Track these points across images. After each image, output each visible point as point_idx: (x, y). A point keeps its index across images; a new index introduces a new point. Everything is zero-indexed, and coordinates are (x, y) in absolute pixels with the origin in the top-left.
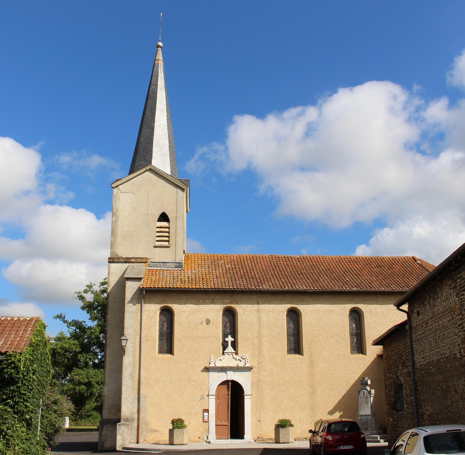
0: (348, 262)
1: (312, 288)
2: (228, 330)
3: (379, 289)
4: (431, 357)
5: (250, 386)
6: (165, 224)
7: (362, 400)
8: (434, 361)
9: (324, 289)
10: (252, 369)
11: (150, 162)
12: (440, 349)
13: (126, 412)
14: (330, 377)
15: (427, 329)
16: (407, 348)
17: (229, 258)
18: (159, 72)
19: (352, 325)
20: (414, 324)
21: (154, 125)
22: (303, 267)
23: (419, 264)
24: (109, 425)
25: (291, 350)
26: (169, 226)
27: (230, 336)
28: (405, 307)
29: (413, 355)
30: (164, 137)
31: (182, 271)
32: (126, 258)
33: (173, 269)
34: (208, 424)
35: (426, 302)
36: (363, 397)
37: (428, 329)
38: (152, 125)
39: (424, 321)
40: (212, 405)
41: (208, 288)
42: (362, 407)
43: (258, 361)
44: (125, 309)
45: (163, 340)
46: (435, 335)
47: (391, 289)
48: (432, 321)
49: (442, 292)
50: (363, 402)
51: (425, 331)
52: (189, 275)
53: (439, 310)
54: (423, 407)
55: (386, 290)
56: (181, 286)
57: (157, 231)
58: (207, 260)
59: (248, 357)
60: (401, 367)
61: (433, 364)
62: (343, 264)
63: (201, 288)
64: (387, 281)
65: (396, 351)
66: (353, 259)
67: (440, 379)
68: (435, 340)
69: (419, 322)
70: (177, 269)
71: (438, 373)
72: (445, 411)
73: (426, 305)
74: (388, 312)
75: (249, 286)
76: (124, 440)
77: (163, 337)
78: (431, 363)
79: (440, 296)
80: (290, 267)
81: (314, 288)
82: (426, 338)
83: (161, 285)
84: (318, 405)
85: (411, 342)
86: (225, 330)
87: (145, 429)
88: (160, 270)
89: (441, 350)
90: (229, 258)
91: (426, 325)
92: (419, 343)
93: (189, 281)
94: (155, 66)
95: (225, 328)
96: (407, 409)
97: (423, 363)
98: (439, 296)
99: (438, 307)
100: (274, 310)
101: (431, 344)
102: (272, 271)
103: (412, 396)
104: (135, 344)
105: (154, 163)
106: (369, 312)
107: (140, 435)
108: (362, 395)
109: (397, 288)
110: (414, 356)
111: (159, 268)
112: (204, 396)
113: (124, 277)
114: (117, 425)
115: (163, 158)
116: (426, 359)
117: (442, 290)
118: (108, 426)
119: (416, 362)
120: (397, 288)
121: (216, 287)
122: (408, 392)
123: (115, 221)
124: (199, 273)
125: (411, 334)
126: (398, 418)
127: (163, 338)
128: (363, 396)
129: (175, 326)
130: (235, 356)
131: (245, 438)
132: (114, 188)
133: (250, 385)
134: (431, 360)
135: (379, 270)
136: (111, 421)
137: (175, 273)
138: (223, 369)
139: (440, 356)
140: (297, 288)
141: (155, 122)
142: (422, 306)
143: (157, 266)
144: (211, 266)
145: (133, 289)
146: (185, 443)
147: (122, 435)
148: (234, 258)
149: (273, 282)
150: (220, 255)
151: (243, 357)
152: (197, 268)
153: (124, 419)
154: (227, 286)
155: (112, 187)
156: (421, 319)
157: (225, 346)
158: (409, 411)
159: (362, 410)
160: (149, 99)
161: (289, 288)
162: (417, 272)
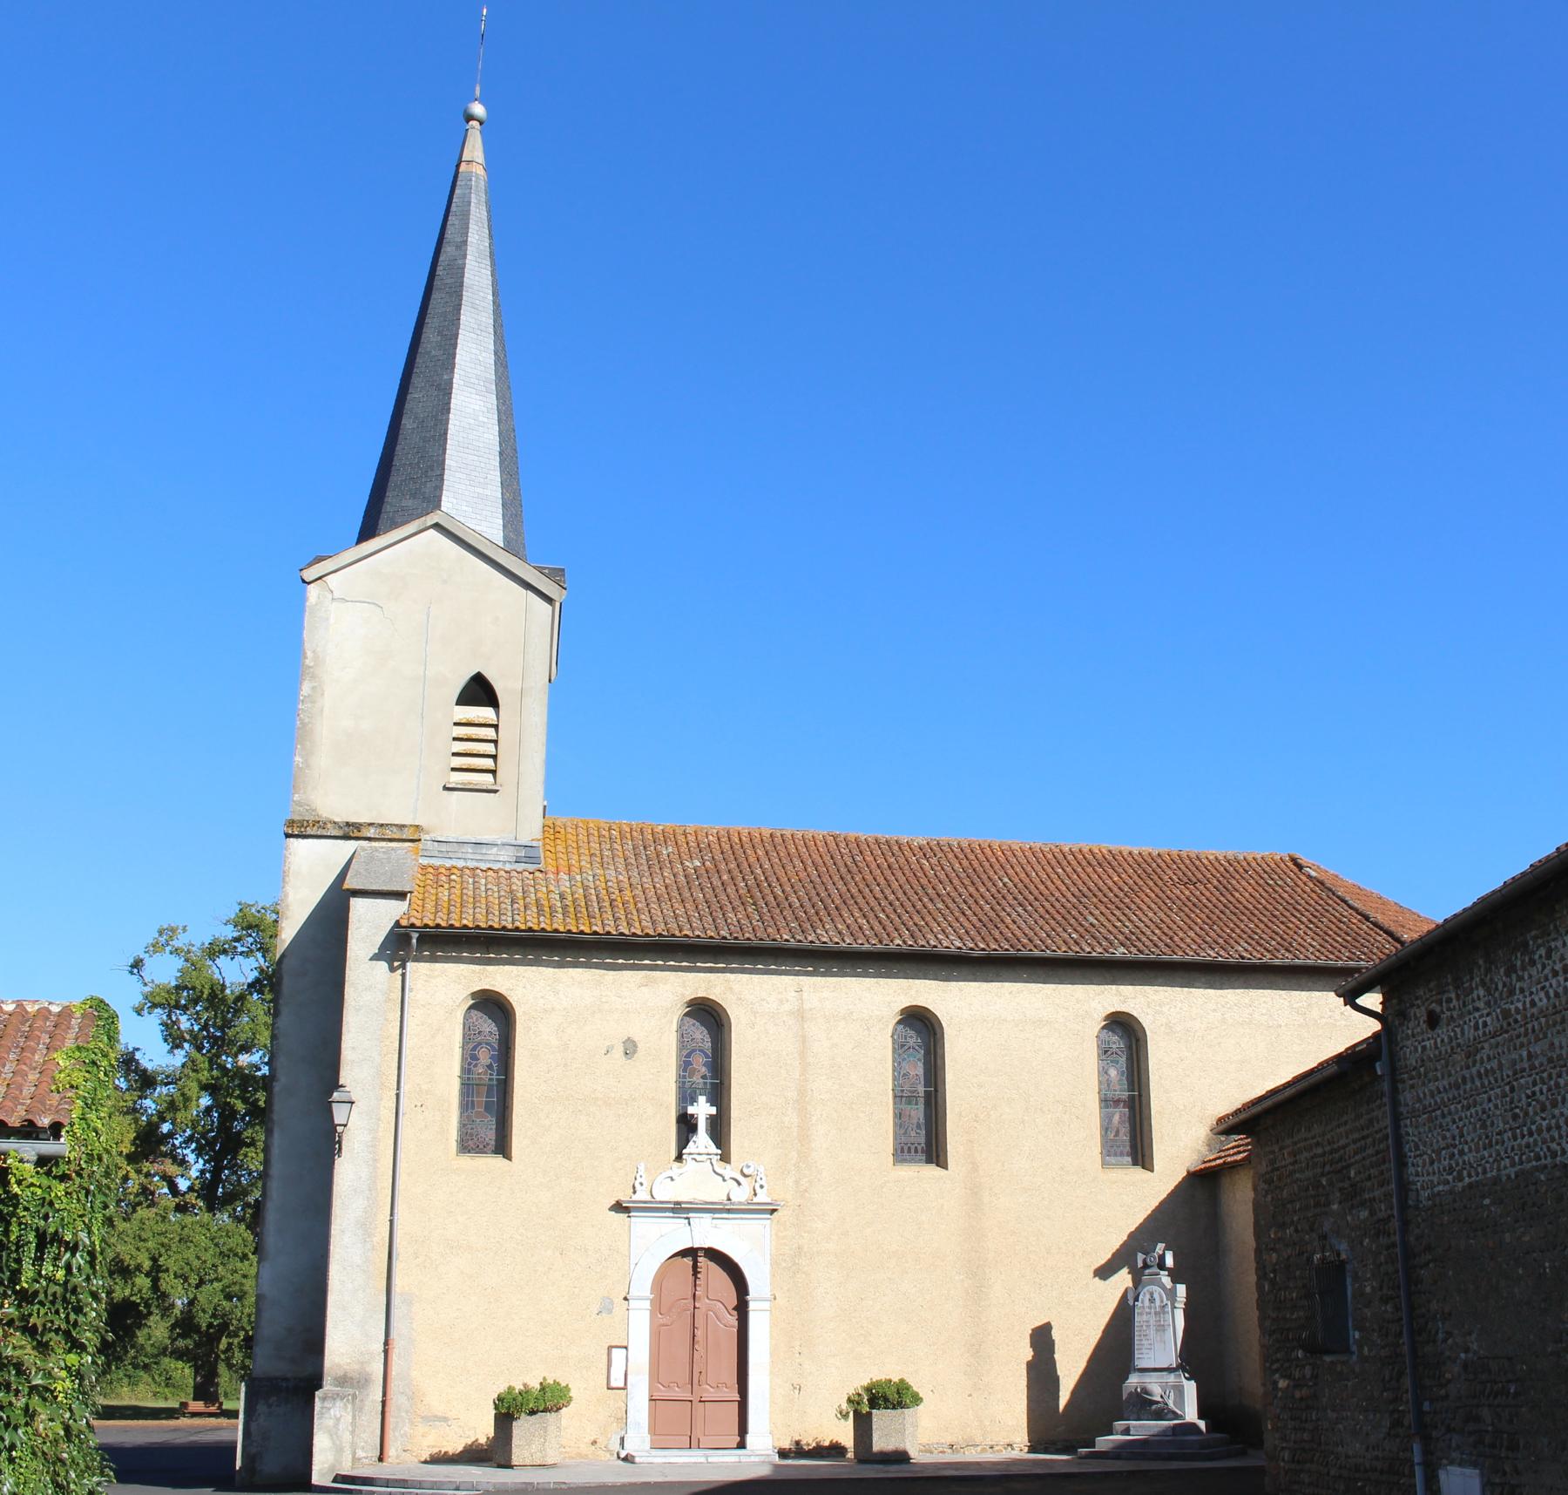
0: (1084, 863)
1: (982, 946)
2: (697, 1079)
3: (1198, 955)
4: (1488, 1166)
5: (767, 1268)
6: (486, 713)
7: (1145, 1318)
8: (1504, 1179)
9: (1008, 950)
10: (775, 1210)
11: (434, 502)
12: (1531, 1140)
13: (343, 1354)
14: (1034, 1243)
15: (1474, 1070)
16: (1370, 1139)
17: (693, 839)
18: (472, 204)
19: (1106, 1073)
20: (1410, 1055)
21: (452, 379)
22: (942, 876)
23: (1315, 878)
24: (275, 1398)
25: (913, 1151)
26: (498, 721)
27: (702, 1099)
28: (1373, 1000)
29: (1402, 1163)
30: (486, 420)
31: (537, 874)
32: (348, 824)
33: (508, 867)
34: (624, 1398)
35: (1472, 979)
36: (1148, 1310)
37: (1479, 1072)
38: (445, 377)
39: (1459, 1045)
40: (639, 1326)
41: (634, 935)
42: (1143, 1342)
43: (797, 1182)
44: (346, 997)
45: (473, 1108)
46: (1512, 1090)
47: (1237, 956)
48: (1498, 1044)
49: (1553, 944)
50: (1148, 1326)
51: (1464, 1079)
52: (563, 888)
53: (1533, 1004)
54: (1441, 1336)
55: (1221, 956)
56: (543, 925)
57: (455, 735)
58: (618, 841)
59: (761, 1169)
60: (1340, 1203)
61: (1499, 1188)
62: (1069, 869)
63: (608, 933)
64: (1219, 931)
65: (1319, 1151)
66: (1099, 856)
67: (1527, 1238)
68: (1512, 1109)
69: (1436, 1048)
70: (520, 867)
71: (1517, 1221)
72: (1549, 1350)
73: (1472, 990)
74: (1225, 1030)
75: (770, 930)
76: (339, 1450)
77: (473, 1097)
78: (1484, 1185)
79: (1541, 956)
80: (899, 874)
81: (988, 945)
82: (1465, 1102)
83: (468, 918)
84: (991, 1337)
85: (1397, 1119)
86: (684, 1077)
87: (407, 1412)
88: (461, 870)
89: (1535, 1140)
90: (691, 838)
91: (1468, 1058)
92: (1430, 1120)
93: (565, 907)
94: (458, 183)
95: (684, 1070)
96: (1361, 1347)
97: (1447, 1188)
98: (1537, 957)
99: (1531, 993)
100: (852, 1013)
101: (1488, 1123)
102: (840, 884)
103: (1385, 1300)
104: (379, 1120)
105: (450, 505)
106: (1163, 1028)
107: (390, 1435)
108: (1147, 1303)
109: (1255, 953)
110: (1405, 1165)
111: (461, 864)
112: (612, 1303)
113: (346, 886)
114: (317, 1399)
115: (480, 491)
116: (1465, 1173)
117: (1553, 935)
118: (271, 1401)
119: (1414, 1187)
120: (1255, 953)
121: (659, 930)
122: (1368, 1289)
123: (309, 696)
124: (598, 882)
125: (1395, 1091)
126: (1315, 1377)
127: (473, 1101)
128: (1150, 1308)
129: (516, 1062)
130: (720, 1166)
131: (748, 1446)
132: (309, 583)
133: (769, 1266)
134: (1489, 1175)
135: (1187, 893)
136: (284, 1385)
137: (514, 880)
138: (678, 1209)
139: (1534, 1163)
140: (932, 943)
141: (453, 368)
142: (1453, 995)
143: (450, 855)
144: (633, 861)
145: (374, 931)
146: (550, 1461)
147: (333, 1434)
148: (710, 837)
149: (849, 922)
150: (661, 828)
151: (746, 1171)
152: (589, 866)
153: (335, 1379)
154: (698, 929)
155: (304, 581)
156: (1442, 1041)
157: (686, 1125)
158: (1370, 1350)
159: (1144, 1351)
160: (433, 292)
161: (904, 942)
162: (1310, 905)
